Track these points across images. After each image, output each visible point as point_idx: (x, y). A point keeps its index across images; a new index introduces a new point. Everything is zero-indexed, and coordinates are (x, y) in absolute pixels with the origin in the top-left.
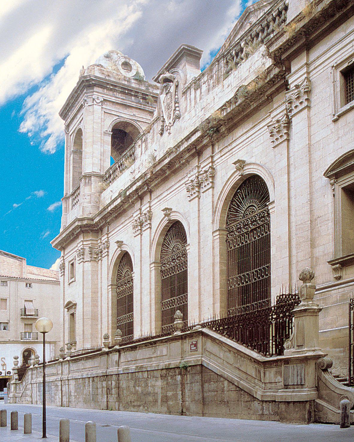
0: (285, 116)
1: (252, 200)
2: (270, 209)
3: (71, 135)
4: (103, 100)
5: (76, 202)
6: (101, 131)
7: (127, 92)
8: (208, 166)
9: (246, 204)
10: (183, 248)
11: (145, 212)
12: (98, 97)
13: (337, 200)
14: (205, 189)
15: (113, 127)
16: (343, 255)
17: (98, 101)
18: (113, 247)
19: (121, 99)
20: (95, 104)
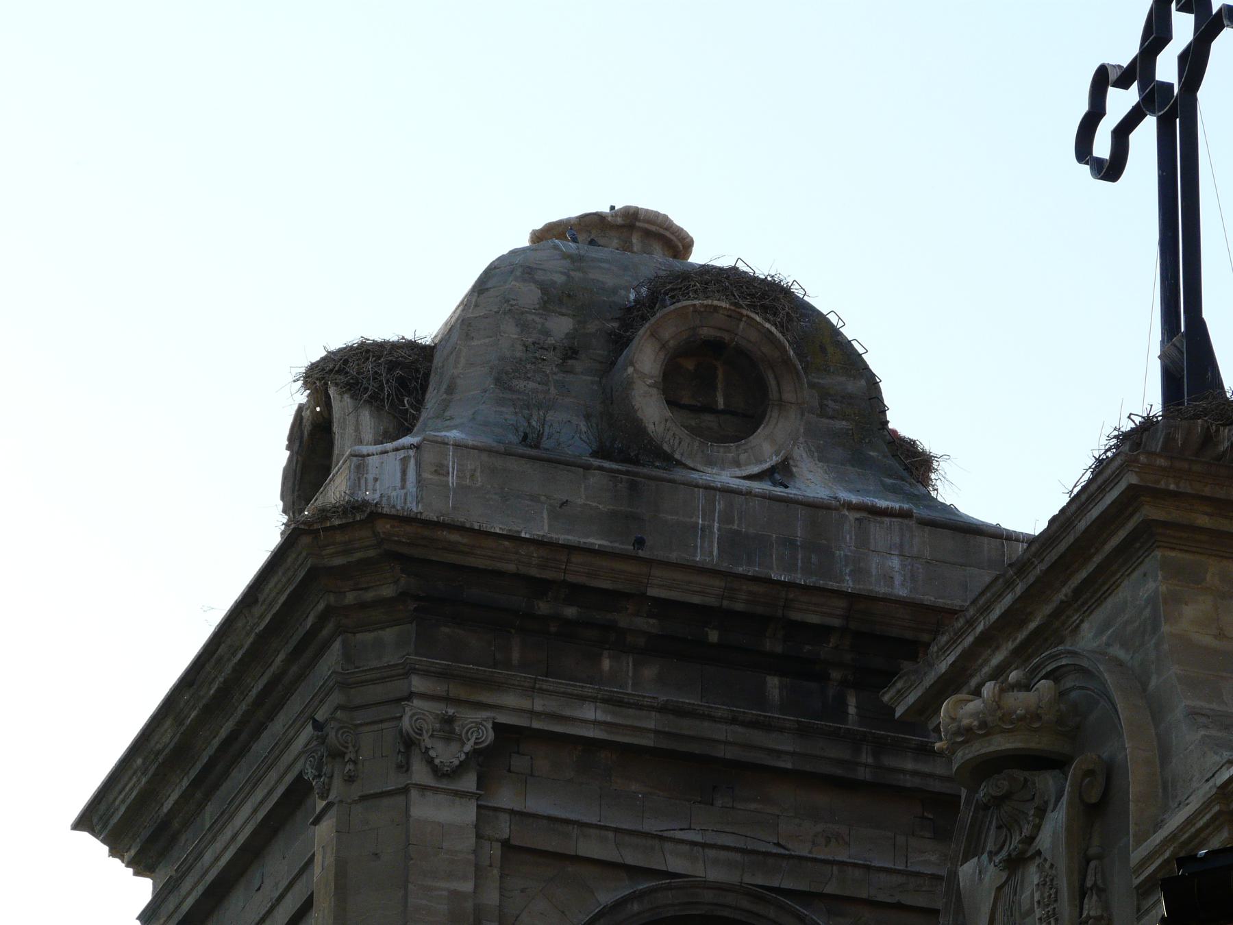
7: (713, 636)
12: (449, 721)
15: (1024, 770)
17: (448, 755)
19: (664, 709)
20: (424, 788)
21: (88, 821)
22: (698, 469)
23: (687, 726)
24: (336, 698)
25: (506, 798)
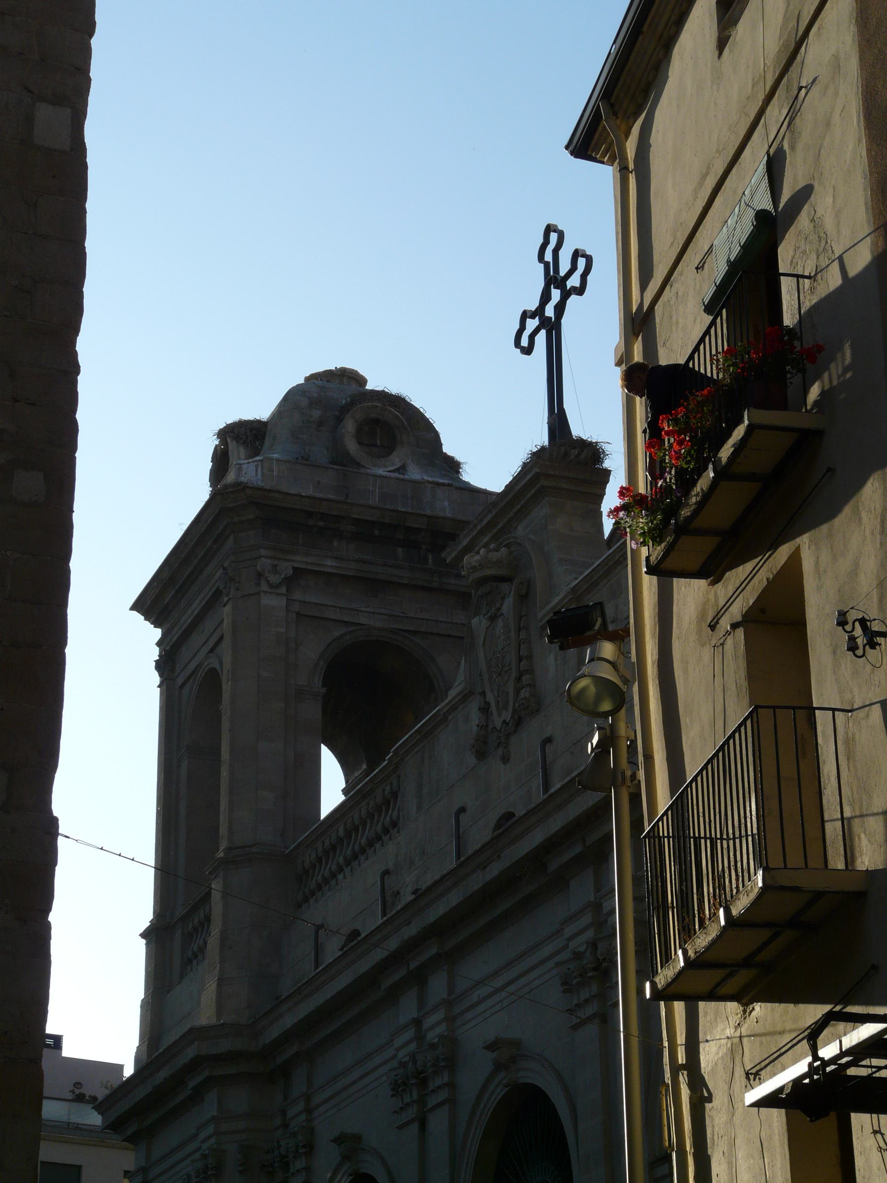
4: (290, 572)
5: (334, 868)
17: (274, 579)
20: (265, 592)
24: (210, 1129)
25: (298, 595)
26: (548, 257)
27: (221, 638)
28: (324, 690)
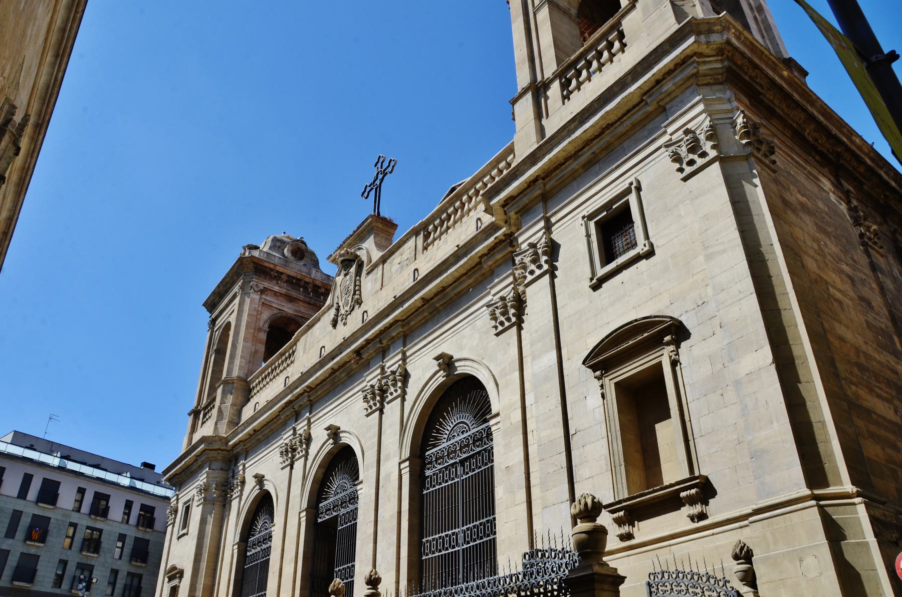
0: (513, 291)
1: (458, 416)
2: (493, 425)
3: (216, 331)
6: (255, 325)
8: (397, 365)
9: (451, 424)
10: (351, 488)
11: (301, 432)
13: (609, 402)
14: (390, 397)
16: (629, 493)
18: (250, 483)
21: (204, 305)
22: (21, 62)
23: (289, 292)
25: (264, 297)
26: (379, 165)
27: (233, 311)
28: (268, 330)
